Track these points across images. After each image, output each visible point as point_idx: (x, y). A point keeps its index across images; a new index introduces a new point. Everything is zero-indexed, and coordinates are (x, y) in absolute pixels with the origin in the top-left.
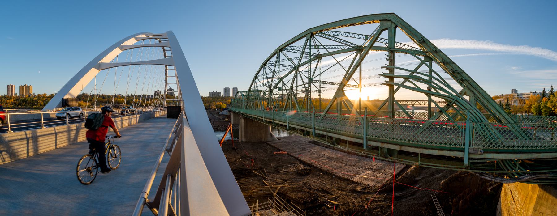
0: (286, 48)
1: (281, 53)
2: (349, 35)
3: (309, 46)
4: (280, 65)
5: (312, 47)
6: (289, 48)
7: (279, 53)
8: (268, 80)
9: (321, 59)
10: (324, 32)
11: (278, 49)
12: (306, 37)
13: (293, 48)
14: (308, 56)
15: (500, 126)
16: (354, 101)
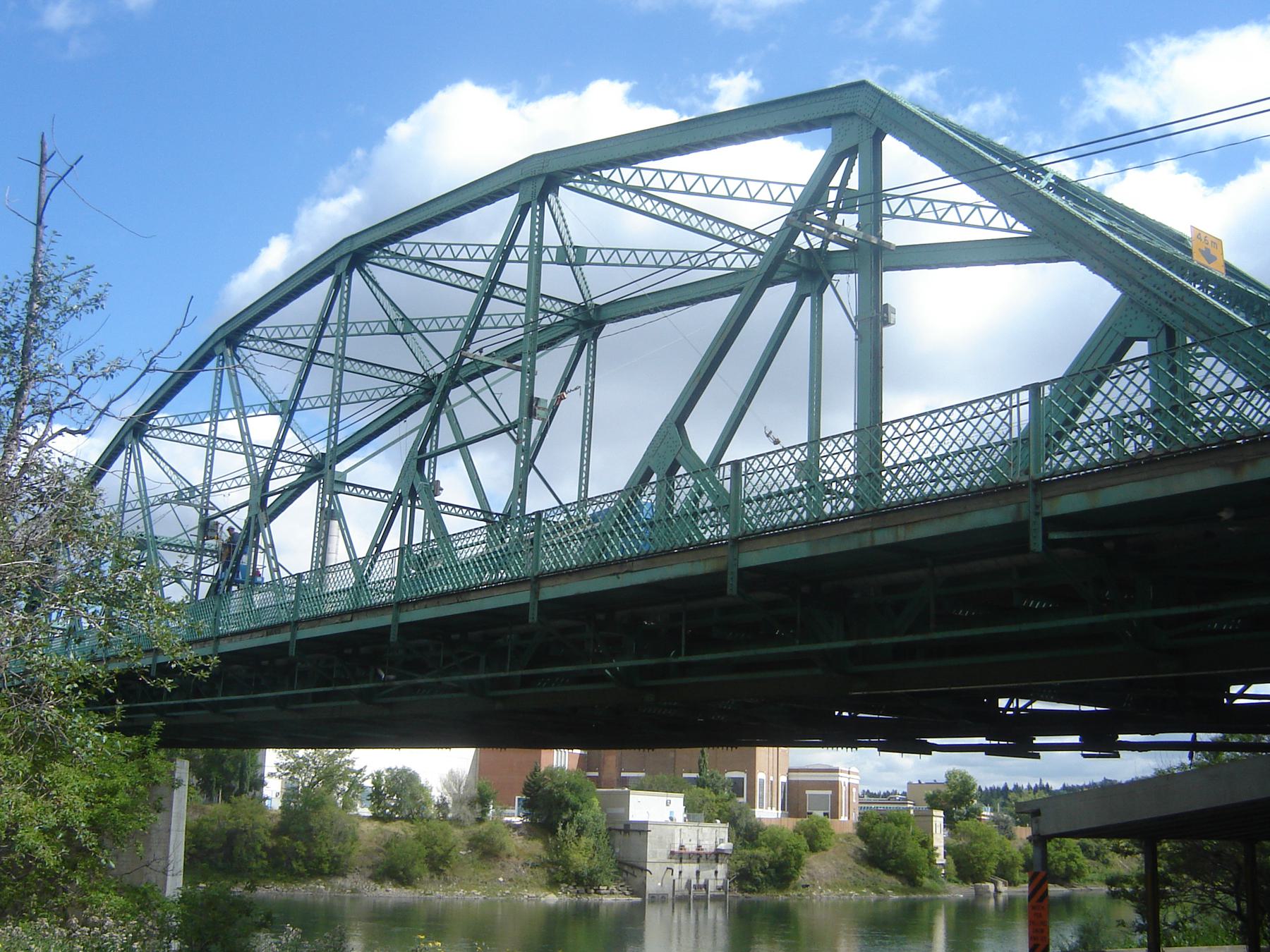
0: (393, 247)
1: (356, 273)
2: (754, 190)
3: (530, 248)
4: (219, 444)
5: (545, 257)
6: (409, 248)
7: (349, 272)
8: (245, 433)
9: (595, 336)
10: (616, 177)
11: (345, 250)
12: (517, 195)
13: (166, 424)
14: (523, 309)
15: (1166, 362)
16: (750, 92)
